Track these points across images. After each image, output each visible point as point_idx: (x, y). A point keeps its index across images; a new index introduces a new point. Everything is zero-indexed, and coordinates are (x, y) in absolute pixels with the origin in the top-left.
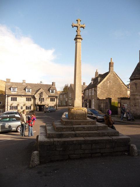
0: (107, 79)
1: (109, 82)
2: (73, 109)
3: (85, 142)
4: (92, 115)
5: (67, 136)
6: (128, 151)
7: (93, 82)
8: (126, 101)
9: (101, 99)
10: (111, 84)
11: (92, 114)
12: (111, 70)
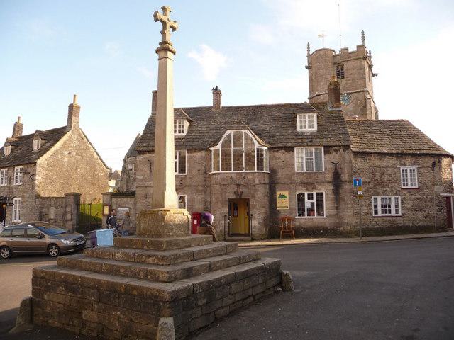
0: (64, 146)
1: (66, 153)
2: (168, 213)
3: (236, 278)
4: (41, 238)
5: (210, 268)
6: (280, 284)
7: (12, 150)
8: (125, 199)
9: (46, 196)
10: (73, 160)
11: (41, 237)
12: (73, 124)
